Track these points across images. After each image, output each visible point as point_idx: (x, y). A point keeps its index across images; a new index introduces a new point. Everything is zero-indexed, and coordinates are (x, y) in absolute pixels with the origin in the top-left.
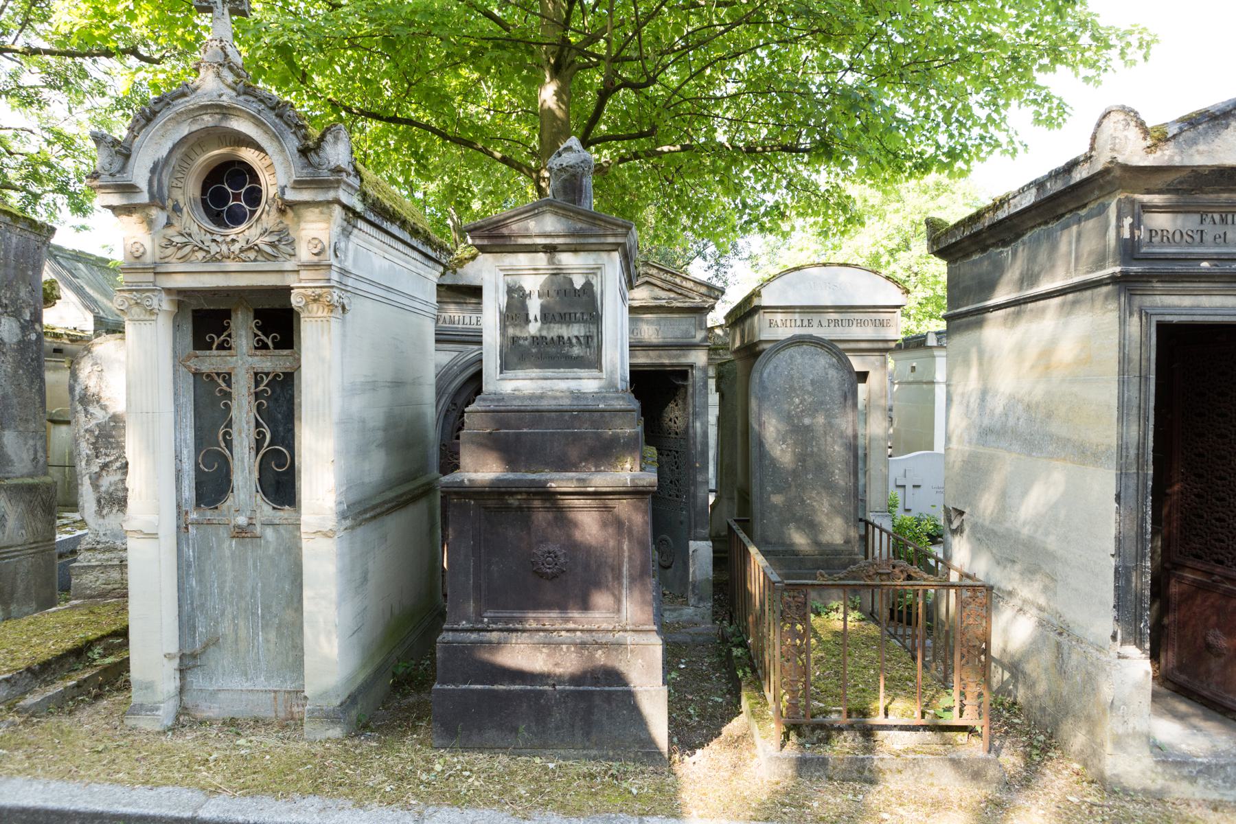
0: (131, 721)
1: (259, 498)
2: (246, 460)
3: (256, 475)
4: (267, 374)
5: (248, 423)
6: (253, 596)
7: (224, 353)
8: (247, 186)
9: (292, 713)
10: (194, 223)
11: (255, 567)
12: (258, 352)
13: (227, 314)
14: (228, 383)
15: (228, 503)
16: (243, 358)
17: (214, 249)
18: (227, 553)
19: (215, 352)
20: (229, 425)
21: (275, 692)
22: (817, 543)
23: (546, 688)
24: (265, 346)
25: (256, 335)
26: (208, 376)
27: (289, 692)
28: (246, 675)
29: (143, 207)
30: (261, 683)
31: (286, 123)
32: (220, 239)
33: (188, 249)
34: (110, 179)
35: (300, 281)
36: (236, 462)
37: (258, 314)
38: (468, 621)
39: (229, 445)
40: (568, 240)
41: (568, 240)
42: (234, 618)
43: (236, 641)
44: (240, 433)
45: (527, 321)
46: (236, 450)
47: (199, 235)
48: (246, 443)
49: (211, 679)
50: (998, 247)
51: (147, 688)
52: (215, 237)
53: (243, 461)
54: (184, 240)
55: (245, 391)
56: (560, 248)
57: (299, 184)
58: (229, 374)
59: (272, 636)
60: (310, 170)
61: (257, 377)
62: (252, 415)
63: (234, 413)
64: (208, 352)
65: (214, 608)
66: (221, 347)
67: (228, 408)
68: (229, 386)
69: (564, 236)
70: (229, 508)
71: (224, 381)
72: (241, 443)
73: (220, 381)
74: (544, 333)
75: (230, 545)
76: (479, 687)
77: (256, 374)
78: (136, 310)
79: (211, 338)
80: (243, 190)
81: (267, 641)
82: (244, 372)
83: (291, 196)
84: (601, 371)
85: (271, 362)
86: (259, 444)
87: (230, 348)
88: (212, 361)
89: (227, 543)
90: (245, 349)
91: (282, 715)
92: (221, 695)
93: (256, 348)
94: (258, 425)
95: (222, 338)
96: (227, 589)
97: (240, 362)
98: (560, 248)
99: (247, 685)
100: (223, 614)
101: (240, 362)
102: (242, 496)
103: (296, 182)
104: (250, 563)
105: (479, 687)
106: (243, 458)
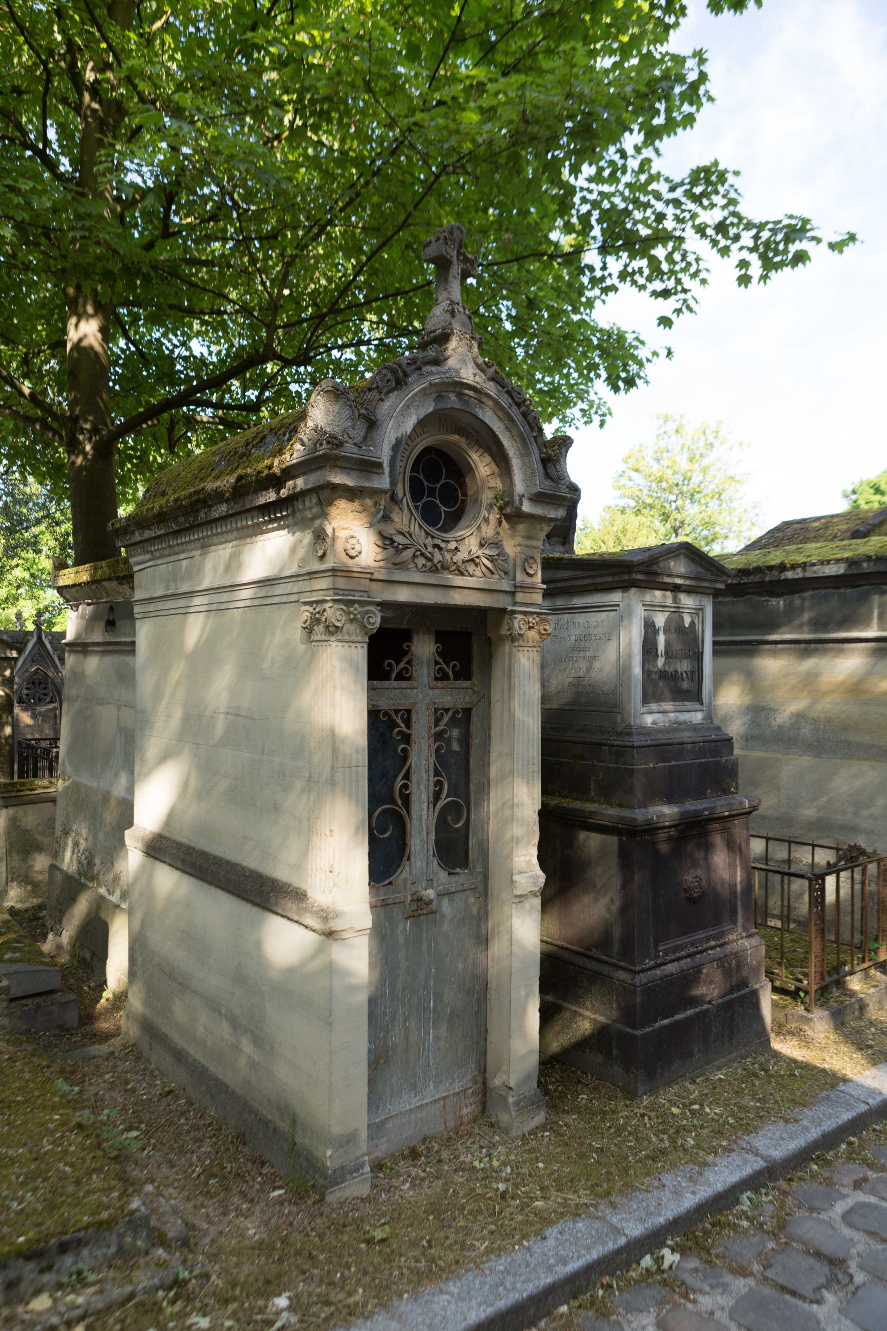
0: (333, 1197)
1: (435, 863)
2: (424, 818)
3: (433, 836)
4: (447, 710)
5: (427, 771)
6: (426, 986)
7: (404, 684)
8: (443, 481)
9: (461, 1117)
10: (404, 519)
11: (429, 949)
12: (440, 684)
13: (406, 635)
14: (408, 723)
15: (405, 875)
16: (425, 694)
17: (437, 557)
18: (401, 939)
19: (395, 684)
20: (407, 776)
21: (444, 1098)
22: (518, 840)
23: (705, 1007)
24: (444, 677)
25: (437, 663)
26: (386, 714)
27: (458, 1094)
28: (415, 1089)
29: (374, 493)
30: (430, 1093)
31: (529, 424)
32: (443, 545)
33: (409, 553)
34: (356, 450)
35: (515, 603)
36: (415, 822)
37: (440, 637)
38: (651, 960)
39: (406, 800)
40: (688, 582)
41: (693, 583)
42: (405, 1021)
43: (406, 1051)
44: (419, 785)
45: (657, 656)
46: (415, 807)
47: (419, 536)
48: (424, 797)
49: (378, 1107)
50: (760, 594)
51: (348, 1142)
52: (439, 542)
53: (420, 820)
54: (406, 541)
55: (424, 733)
56: (683, 588)
57: (538, 498)
58: (409, 711)
59: (443, 1030)
60: (548, 483)
61: (438, 714)
62: (431, 761)
63: (413, 760)
64: (387, 683)
65: (385, 1013)
66: (400, 677)
67: (405, 756)
68: (408, 726)
69: (688, 578)
70: (405, 880)
71: (404, 721)
72: (419, 799)
73: (399, 721)
74: (667, 668)
75: (405, 927)
76: (666, 1022)
77: (436, 710)
78: (352, 628)
79: (389, 665)
80: (438, 485)
81: (437, 1038)
82: (424, 708)
83: (527, 507)
84: (702, 704)
85: (450, 697)
86: (437, 796)
87: (409, 679)
88: (395, 696)
89: (401, 926)
90: (425, 680)
91: (451, 1124)
92: (389, 1125)
93: (436, 679)
94: (437, 773)
95: (402, 665)
96: (400, 986)
97: (421, 696)
98: (683, 588)
99: (416, 1102)
100: (394, 1019)
101: (421, 696)
102: (419, 864)
103: (539, 493)
104: (424, 946)
105: (666, 1022)
106: (421, 816)
